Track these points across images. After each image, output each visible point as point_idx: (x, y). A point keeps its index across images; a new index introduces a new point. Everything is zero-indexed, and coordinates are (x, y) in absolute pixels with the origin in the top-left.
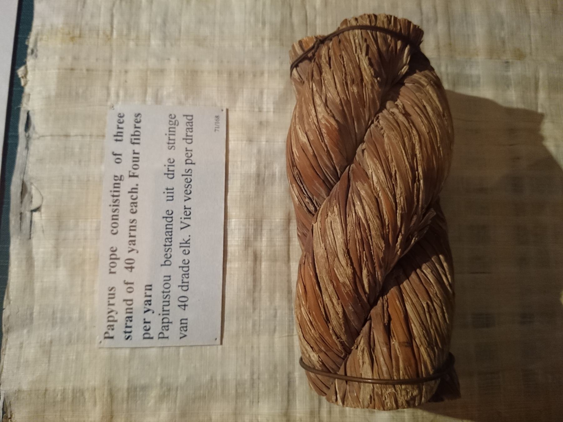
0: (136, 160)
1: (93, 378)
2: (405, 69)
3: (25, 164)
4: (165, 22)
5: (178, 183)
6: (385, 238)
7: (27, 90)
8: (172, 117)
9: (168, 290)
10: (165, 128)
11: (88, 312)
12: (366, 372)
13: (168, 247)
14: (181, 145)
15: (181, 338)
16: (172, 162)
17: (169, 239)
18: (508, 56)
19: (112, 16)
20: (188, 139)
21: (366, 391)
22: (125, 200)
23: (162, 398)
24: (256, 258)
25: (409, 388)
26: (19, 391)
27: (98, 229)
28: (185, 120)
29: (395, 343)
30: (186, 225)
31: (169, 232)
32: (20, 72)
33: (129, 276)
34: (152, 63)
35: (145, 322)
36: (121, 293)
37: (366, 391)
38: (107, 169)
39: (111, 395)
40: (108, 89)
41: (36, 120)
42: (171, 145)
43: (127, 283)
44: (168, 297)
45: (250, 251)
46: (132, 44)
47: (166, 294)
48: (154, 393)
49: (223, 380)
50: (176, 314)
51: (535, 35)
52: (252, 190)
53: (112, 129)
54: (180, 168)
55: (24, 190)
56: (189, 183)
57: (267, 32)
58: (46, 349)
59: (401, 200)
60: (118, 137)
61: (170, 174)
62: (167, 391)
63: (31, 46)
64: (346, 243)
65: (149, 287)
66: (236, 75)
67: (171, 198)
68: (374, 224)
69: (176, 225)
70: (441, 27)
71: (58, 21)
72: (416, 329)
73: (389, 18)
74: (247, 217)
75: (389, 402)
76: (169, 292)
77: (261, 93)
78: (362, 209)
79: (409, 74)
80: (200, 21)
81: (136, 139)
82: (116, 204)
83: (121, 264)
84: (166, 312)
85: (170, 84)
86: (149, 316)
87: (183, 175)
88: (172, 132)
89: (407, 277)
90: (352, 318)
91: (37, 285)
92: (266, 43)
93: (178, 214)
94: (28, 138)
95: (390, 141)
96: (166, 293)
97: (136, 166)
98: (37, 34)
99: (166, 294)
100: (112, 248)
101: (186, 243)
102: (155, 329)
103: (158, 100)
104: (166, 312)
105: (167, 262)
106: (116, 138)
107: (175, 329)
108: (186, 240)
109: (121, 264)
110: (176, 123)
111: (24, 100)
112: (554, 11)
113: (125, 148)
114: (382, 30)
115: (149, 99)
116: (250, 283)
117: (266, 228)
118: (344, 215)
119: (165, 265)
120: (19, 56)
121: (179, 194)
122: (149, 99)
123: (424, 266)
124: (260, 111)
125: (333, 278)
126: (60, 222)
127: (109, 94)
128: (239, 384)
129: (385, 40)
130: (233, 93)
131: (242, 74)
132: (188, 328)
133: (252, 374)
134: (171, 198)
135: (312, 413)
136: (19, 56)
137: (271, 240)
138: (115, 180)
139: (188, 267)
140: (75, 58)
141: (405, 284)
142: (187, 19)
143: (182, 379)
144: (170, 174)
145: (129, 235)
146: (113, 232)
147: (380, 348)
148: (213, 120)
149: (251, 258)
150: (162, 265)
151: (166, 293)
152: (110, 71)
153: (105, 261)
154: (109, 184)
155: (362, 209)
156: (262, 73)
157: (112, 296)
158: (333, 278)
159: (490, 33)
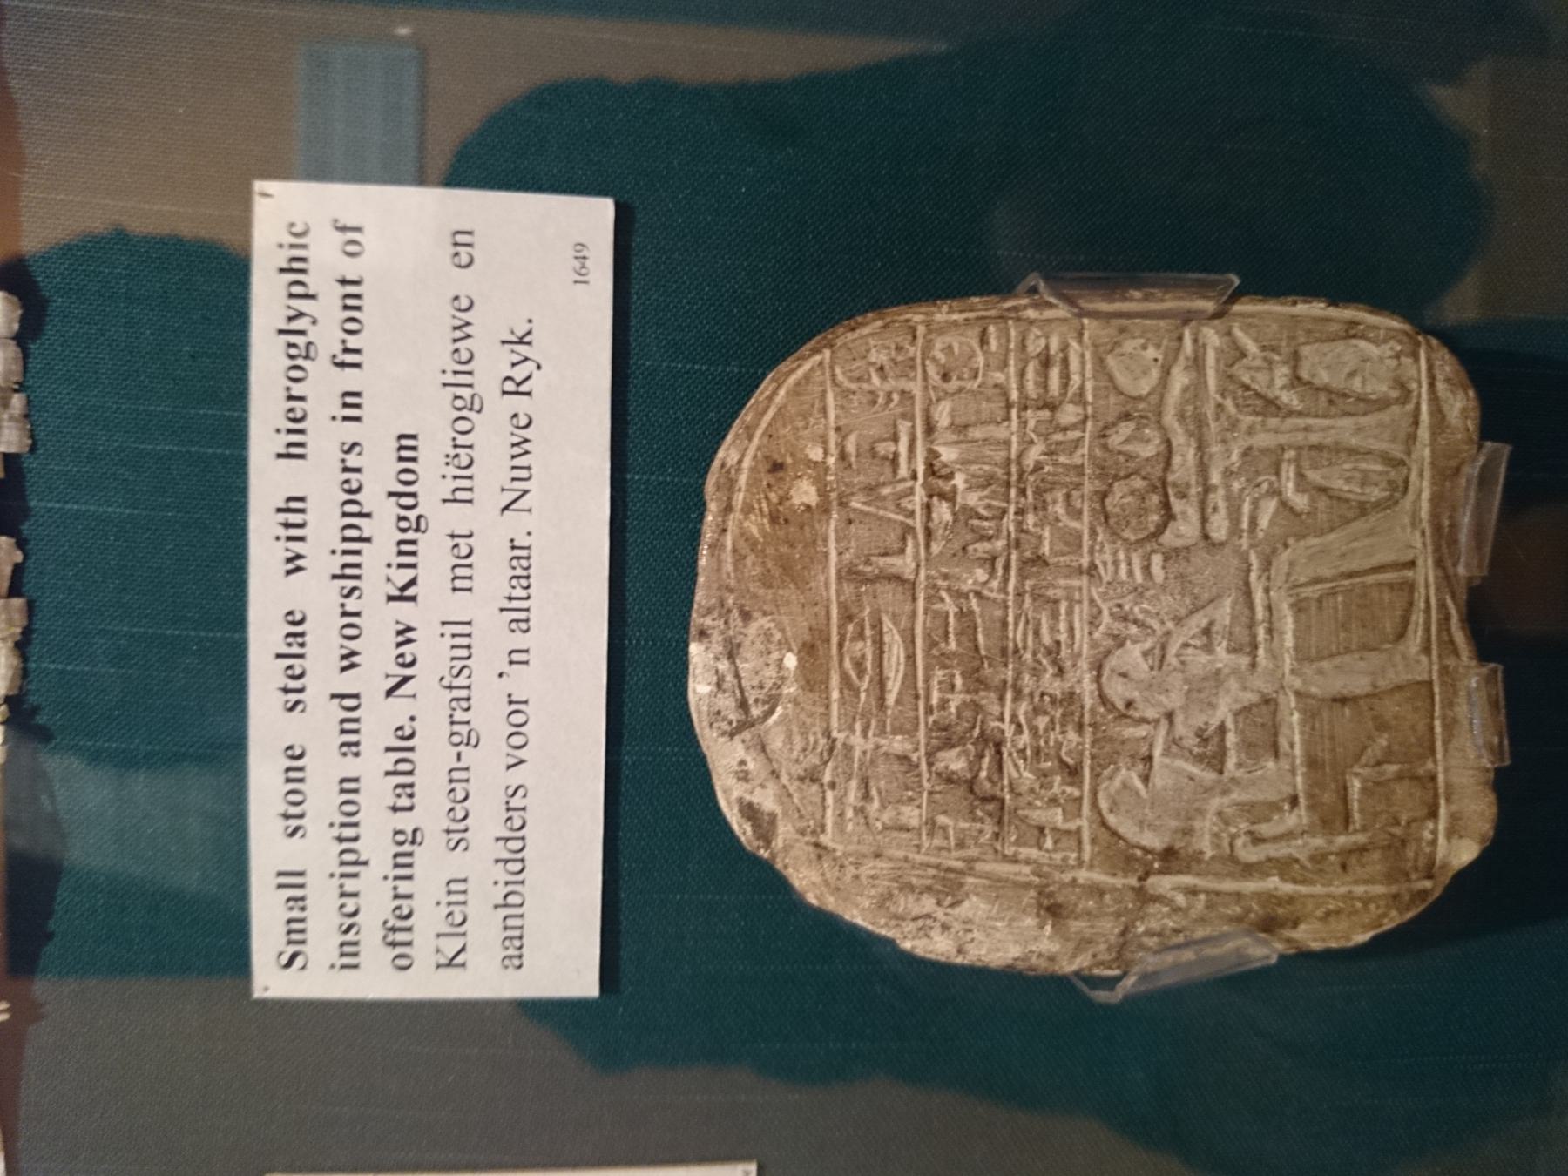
9: (461, 826)
15: (509, 767)
25: (1179, 543)
30: (514, 506)
35: (396, 897)
43: (344, 229)
44: (466, 672)
47: (456, 837)
67: (454, 887)
76: (466, 830)
87: (503, 342)
99: (456, 837)
100: (290, 613)
101: (521, 342)
106: (282, 517)
108: (520, 333)
119: (455, 501)
132: (525, 940)
138: (292, 357)
139: (522, 860)
145: (340, 610)
146: (294, 230)
150: (445, 501)
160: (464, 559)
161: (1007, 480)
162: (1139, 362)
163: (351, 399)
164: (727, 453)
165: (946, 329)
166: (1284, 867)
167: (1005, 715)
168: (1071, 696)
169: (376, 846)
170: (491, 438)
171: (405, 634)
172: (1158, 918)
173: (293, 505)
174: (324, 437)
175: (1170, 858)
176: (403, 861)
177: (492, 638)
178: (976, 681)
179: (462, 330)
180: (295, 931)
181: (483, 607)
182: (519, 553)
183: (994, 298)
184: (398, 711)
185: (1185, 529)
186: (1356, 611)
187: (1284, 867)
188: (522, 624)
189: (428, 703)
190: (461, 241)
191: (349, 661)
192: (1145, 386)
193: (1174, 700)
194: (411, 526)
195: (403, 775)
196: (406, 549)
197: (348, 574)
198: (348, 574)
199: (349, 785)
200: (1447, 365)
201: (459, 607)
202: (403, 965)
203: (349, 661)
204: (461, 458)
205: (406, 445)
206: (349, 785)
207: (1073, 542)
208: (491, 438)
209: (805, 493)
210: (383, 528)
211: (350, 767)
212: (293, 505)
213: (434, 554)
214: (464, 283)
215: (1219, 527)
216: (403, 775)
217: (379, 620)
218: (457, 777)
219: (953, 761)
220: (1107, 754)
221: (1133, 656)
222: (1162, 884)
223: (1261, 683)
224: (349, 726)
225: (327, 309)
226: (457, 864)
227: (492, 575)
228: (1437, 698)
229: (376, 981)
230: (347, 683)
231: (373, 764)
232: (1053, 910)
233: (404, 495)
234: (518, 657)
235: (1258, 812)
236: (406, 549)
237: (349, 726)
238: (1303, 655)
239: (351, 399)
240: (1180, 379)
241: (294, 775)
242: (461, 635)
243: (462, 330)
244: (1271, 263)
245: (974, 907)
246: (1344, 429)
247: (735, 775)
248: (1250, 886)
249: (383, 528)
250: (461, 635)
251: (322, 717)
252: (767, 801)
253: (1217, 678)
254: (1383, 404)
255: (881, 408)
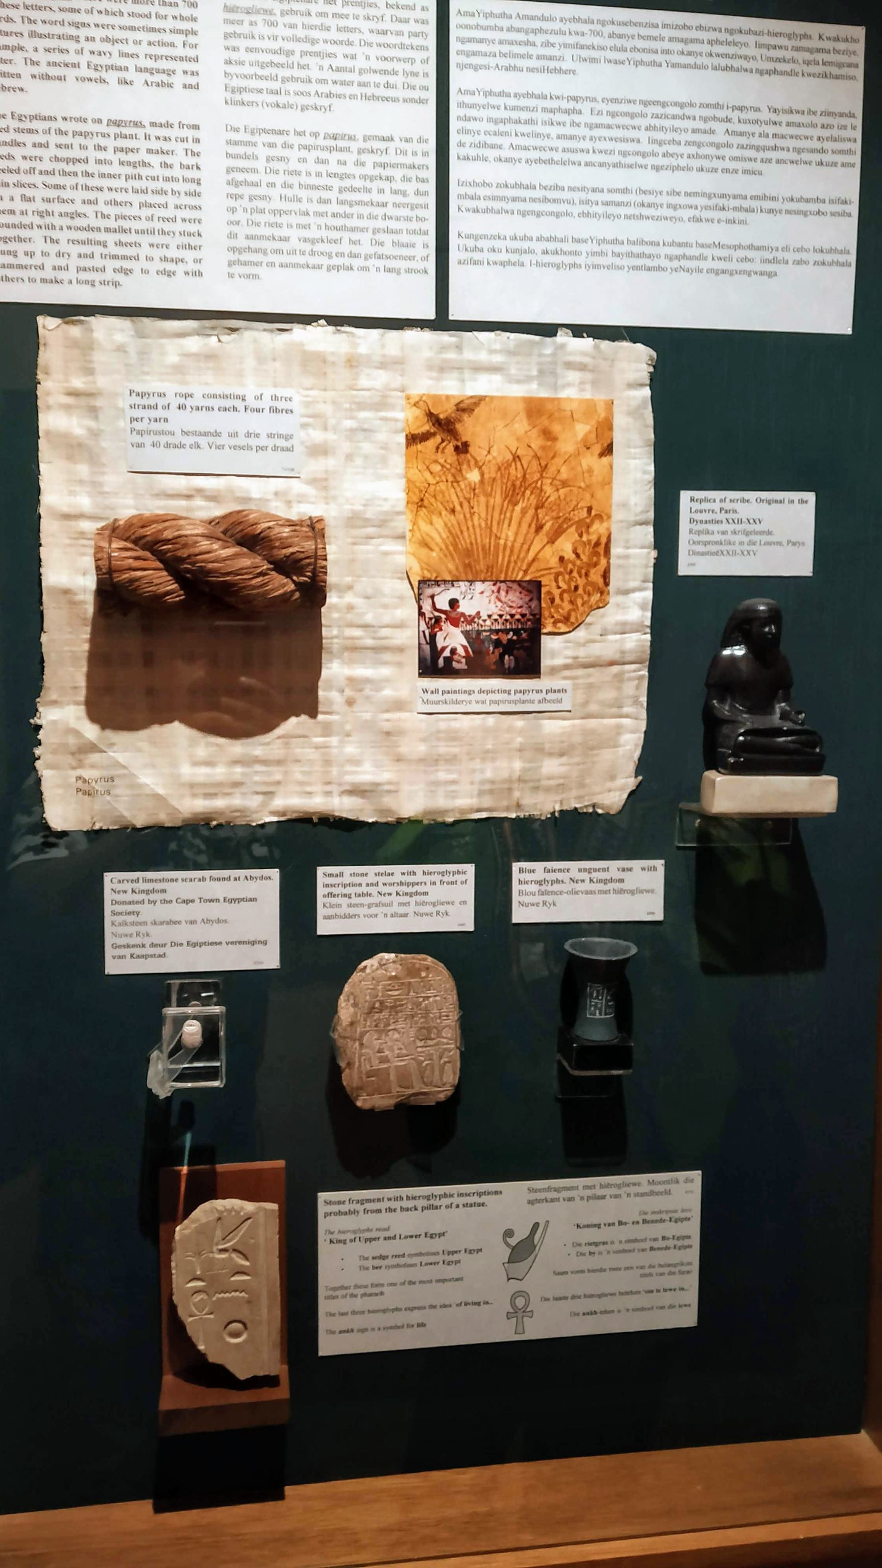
0: (258, 411)
1: (102, 382)
2: (295, 578)
3: (252, 329)
4: (365, 430)
5: (242, 441)
6: (189, 556)
7: (308, 327)
8: (291, 436)
10: (283, 431)
11: (148, 378)
12: (114, 545)
13: (195, 433)
14: (270, 443)
16: (257, 436)
17: (201, 434)
18: (348, 692)
19: (369, 390)
20: (275, 448)
21: (106, 545)
22: (228, 403)
23: (90, 430)
24: (189, 497)
26: (92, 331)
27: (206, 384)
28: (289, 446)
29: (131, 561)
31: (205, 434)
32: (322, 322)
33: (174, 406)
34: (332, 422)
36: (161, 402)
37: (106, 545)
38: (250, 390)
39: (91, 395)
40: (311, 389)
41: (285, 336)
42: (270, 436)
45: (192, 493)
46: (348, 406)
48: (92, 424)
49: (103, 473)
50: (148, 440)
51: (367, 716)
52: (239, 495)
53: (280, 392)
54: (253, 442)
55: (233, 330)
56: (242, 448)
57: (358, 507)
58: (121, 349)
59: (210, 566)
60: (275, 398)
61: (248, 435)
62: (95, 434)
63: (343, 329)
64: (186, 536)
65: (166, 420)
66: (324, 484)
68: (196, 550)
69: (211, 439)
70: (369, 642)
71: (363, 350)
72: (139, 574)
73: (325, 567)
74: (219, 491)
75: (99, 556)
77: (313, 503)
78: (205, 544)
79: (294, 581)
80: (366, 457)
81: (274, 410)
82: (225, 397)
83: (182, 401)
84: (149, 432)
85: (317, 436)
86: (146, 421)
88: (280, 436)
89: (170, 575)
90: (144, 541)
91: (164, 341)
92: (349, 507)
93: (219, 441)
94: (271, 331)
95: (246, 562)
96: (163, 433)
97: (252, 410)
98: (352, 333)
102: (138, 426)
103: (304, 426)
104: (149, 432)
105: (185, 433)
107: (137, 439)
109: (182, 401)
110: (286, 439)
111: (301, 326)
112: (388, 734)
113: (266, 403)
114: (315, 563)
115: (306, 420)
116: (170, 492)
117: (212, 504)
118: (203, 536)
120: (335, 321)
121: (233, 441)
122: (306, 420)
123: (176, 585)
124: (299, 502)
125: (165, 529)
126: (210, 356)
127: (307, 389)
128: (101, 484)
129: (309, 564)
130: (313, 482)
131: (326, 488)
133: (107, 493)
134: (230, 435)
135: (82, 533)
136: (335, 321)
137: (201, 508)
140: (333, 363)
141: (165, 573)
142: (367, 447)
143: (104, 444)
144: (248, 435)
147: (128, 554)
148: (291, 467)
149: (189, 493)
151: (163, 433)
152: (325, 390)
153: (184, 390)
154: (239, 391)
155: (205, 544)
156: (327, 504)
157: (160, 395)
158: (165, 529)
159: (368, 681)
160: (404, 904)
161: (427, 1011)
162: (448, 1033)
163: (434, 883)
164: (430, 959)
165: (453, 997)
166: (360, 1066)
167: (385, 1014)
168: (389, 1025)
169: (348, 890)
170: (428, 909)
171: (390, 894)
172: (350, 1043)
173: (414, 873)
174: (427, 879)
175: (361, 1044)
176: (345, 895)
177: (389, 910)
178: (392, 1007)
179: (448, 903)
180: (331, 875)
181: (396, 909)
182: (406, 915)
183: (413, 1101)
184: (375, 893)
185: (419, 1044)
186: (404, 1076)
187: (360, 1066)
188: (392, 916)
189: (376, 899)
190: (465, 902)
191: (385, 884)
192: (444, 1035)
193: (389, 1044)
194: (411, 895)
195: (363, 895)
196: (407, 894)
197: (401, 884)
198: (401, 884)
199: (360, 885)
200: (449, 1093)
201: (395, 904)
202: (324, 896)
203: (385, 884)
204: (424, 903)
205: (426, 894)
206: (360, 885)
207: (416, 1023)
208: (428, 909)
209: (423, 974)
210: (411, 889)
211: (364, 885)
212: (414, 873)
213: (406, 899)
214: (457, 904)
215: (419, 1050)
216: (363, 895)
217: (392, 890)
218: (362, 905)
219: (377, 1005)
220: (380, 1032)
221: (396, 1036)
222: (357, 1044)
223: (392, 1060)
224: (372, 885)
225: (451, 878)
226: (344, 906)
227: (402, 910)
228: (227, 1295)
229: (321, 891)
230: (380, 884)
231: (364, 889)
232: (352, 1024)
233: (417, 893)
234: (386, 915)
235: (370, 1060)
236: (407, 894)
237: (372, 885)
238: (397, 1067)
239: (434, 883)
240: (445, 1041)
241: (362, 875)
242: (390, 905)
243: (448, 903)
244: (466, 1057)
245: (352, 1010)
246: (437, 1073)
247: (370, 963)
248: (357, 1060)
249: (411, 889)
250: (390, 905)
251: (374, 880)
252: (368, 971)
253: (393, 1051)
254: (441, 1079)
255: (439, 988)
